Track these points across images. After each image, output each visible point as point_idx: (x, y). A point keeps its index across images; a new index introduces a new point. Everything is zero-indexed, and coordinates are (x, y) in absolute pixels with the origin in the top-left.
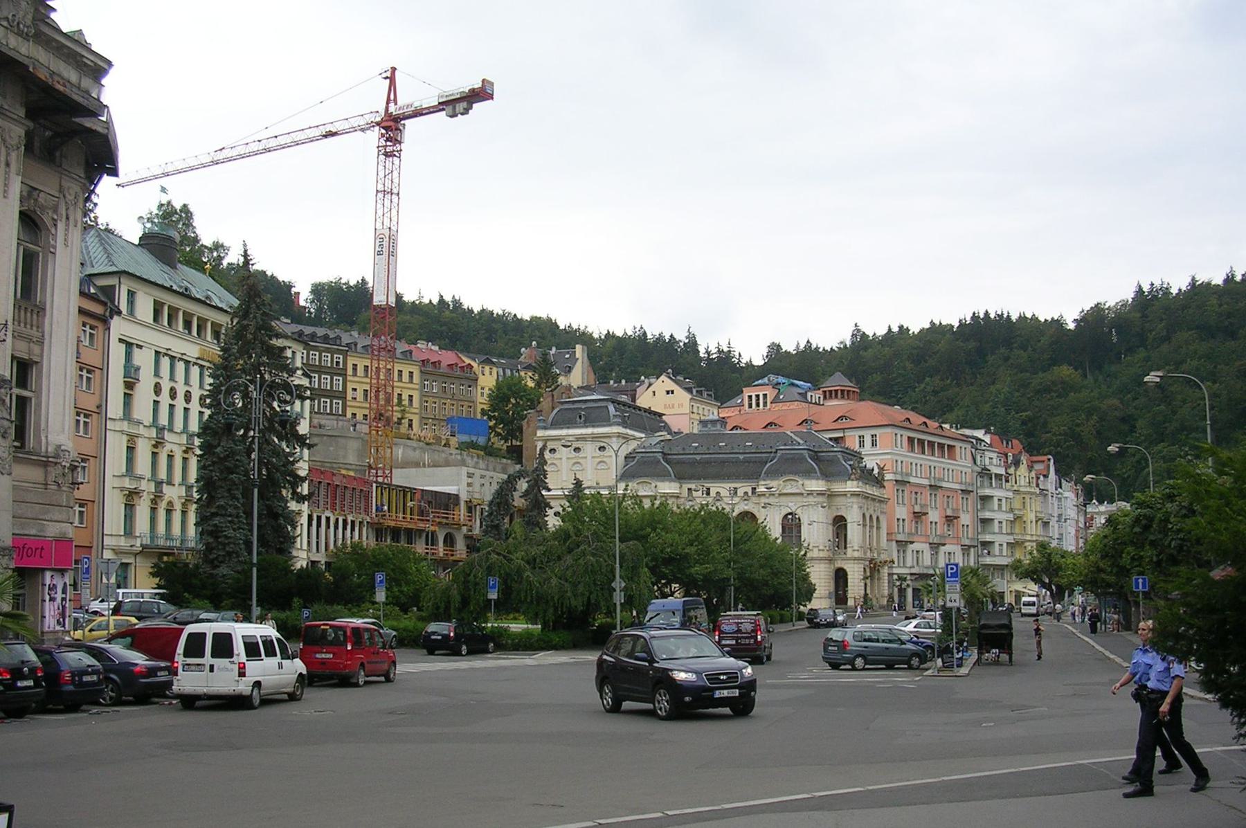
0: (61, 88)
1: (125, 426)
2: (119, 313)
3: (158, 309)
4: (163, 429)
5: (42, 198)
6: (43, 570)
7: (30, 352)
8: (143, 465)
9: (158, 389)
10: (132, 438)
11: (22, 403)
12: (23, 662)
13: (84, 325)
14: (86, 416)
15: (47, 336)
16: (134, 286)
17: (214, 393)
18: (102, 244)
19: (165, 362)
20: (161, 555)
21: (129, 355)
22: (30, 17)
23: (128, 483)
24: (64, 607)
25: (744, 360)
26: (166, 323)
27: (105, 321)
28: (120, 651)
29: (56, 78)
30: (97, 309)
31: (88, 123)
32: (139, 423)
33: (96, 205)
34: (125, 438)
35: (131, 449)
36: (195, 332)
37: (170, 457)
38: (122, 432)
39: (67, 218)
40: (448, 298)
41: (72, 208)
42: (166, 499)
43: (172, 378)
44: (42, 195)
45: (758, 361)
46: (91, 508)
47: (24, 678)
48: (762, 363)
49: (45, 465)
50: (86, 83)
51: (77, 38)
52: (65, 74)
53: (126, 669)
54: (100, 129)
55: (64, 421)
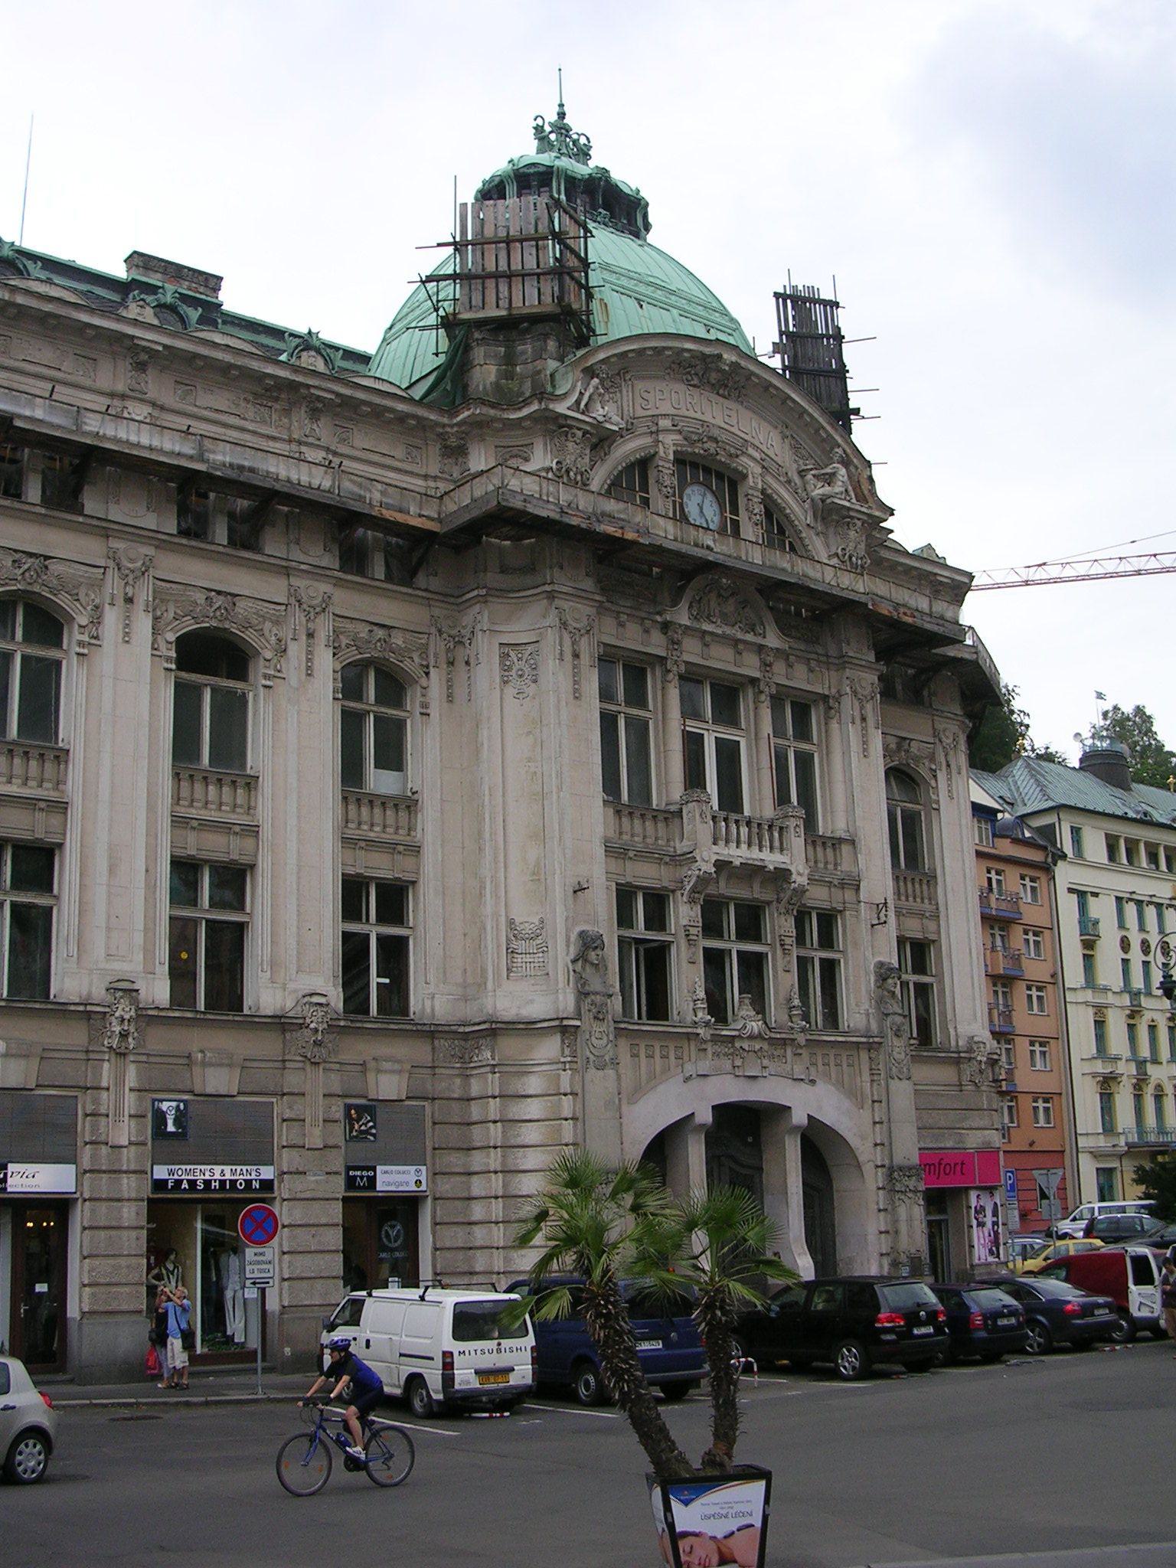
0: (910, 620)
1: (1089, 995)
2: (1064, 857)
4: (1138, 993)
5: (914, 748)
6: (967, 1189)
7: (923, 930)
8: (1118, 1042)
9: (1125, 945)
10: (1100, 1010)
11: (923, 990)
12: (918, 1305)
13: (1023, 878)
14: (1039, 989)
15: (942, 909)
16: (1079, 820)
18: (1032, 776)
19: (1131, 910)
20: (1153, 1155)
21: (1083, 907)
22: (863, 546)
23: (1100, 1067)
24: (996, 1233)
26: (1125, 861)
27: (1047, 869)
28: (1057, 1288)
29: (902, 610)
30: (1036, 856)
31: (951, 652)
32: (1106, 989)
33: (1027, 726)
34: (1091, 1011)
35: (1100, 1024)
36: (1163, 866)
37: (1152, 1028)
38: (1086, 1003)
39: (948, 766)
41: (951, 753)
42: (1153, 1082)
43: (1142, 928)
44: (913, 743)
46: (1056, 1100)
47: (922, 1324)
49: (957, 1062)
50: (940, 607)
51: (927, 556)
52: (912, 603)
53: (1056, 1308)
54: (967, 656)
55: (974, 1006)
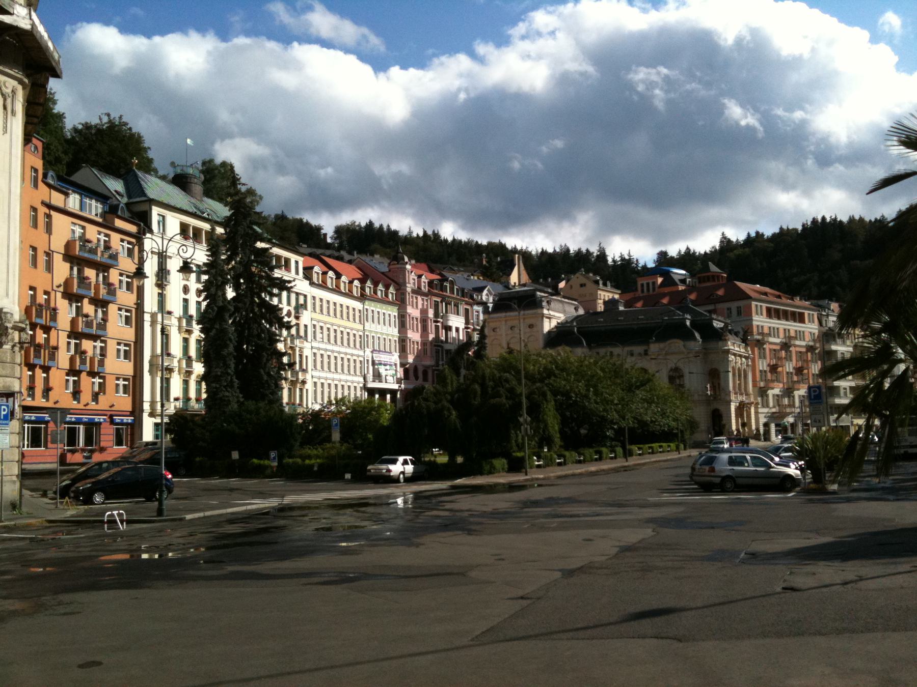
3: (184, 228)
17: (207, 286)
25: (641, 263)
40: (430, 232)
45: (651, 265)
48: (654, 265)
